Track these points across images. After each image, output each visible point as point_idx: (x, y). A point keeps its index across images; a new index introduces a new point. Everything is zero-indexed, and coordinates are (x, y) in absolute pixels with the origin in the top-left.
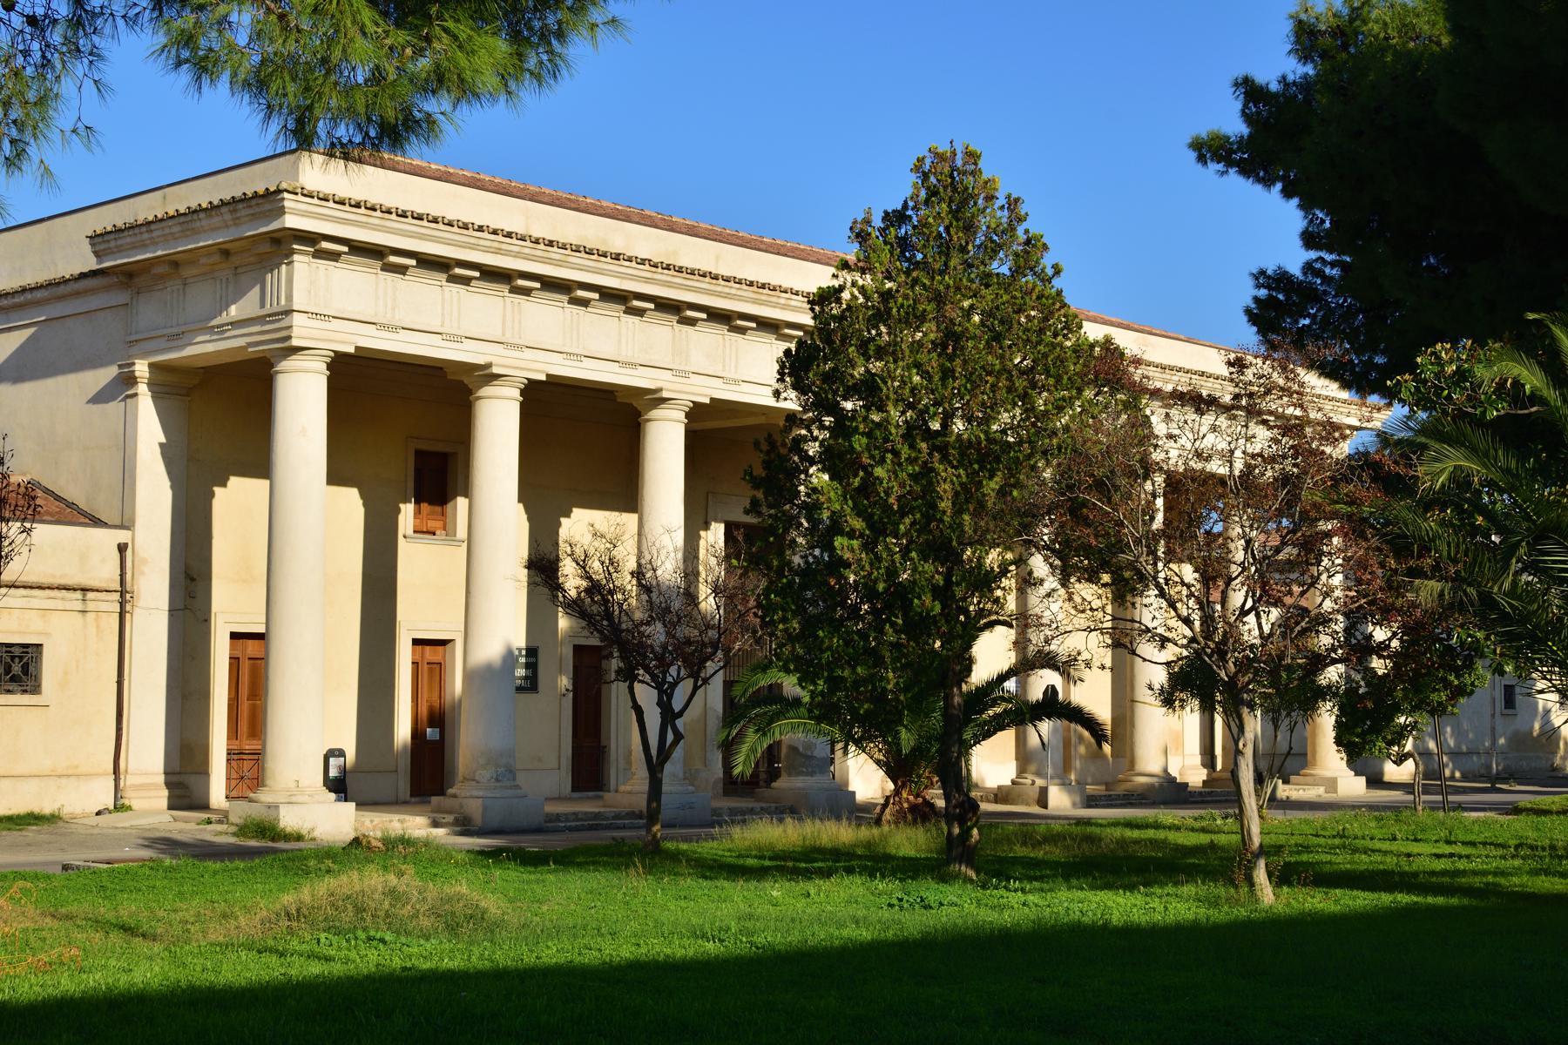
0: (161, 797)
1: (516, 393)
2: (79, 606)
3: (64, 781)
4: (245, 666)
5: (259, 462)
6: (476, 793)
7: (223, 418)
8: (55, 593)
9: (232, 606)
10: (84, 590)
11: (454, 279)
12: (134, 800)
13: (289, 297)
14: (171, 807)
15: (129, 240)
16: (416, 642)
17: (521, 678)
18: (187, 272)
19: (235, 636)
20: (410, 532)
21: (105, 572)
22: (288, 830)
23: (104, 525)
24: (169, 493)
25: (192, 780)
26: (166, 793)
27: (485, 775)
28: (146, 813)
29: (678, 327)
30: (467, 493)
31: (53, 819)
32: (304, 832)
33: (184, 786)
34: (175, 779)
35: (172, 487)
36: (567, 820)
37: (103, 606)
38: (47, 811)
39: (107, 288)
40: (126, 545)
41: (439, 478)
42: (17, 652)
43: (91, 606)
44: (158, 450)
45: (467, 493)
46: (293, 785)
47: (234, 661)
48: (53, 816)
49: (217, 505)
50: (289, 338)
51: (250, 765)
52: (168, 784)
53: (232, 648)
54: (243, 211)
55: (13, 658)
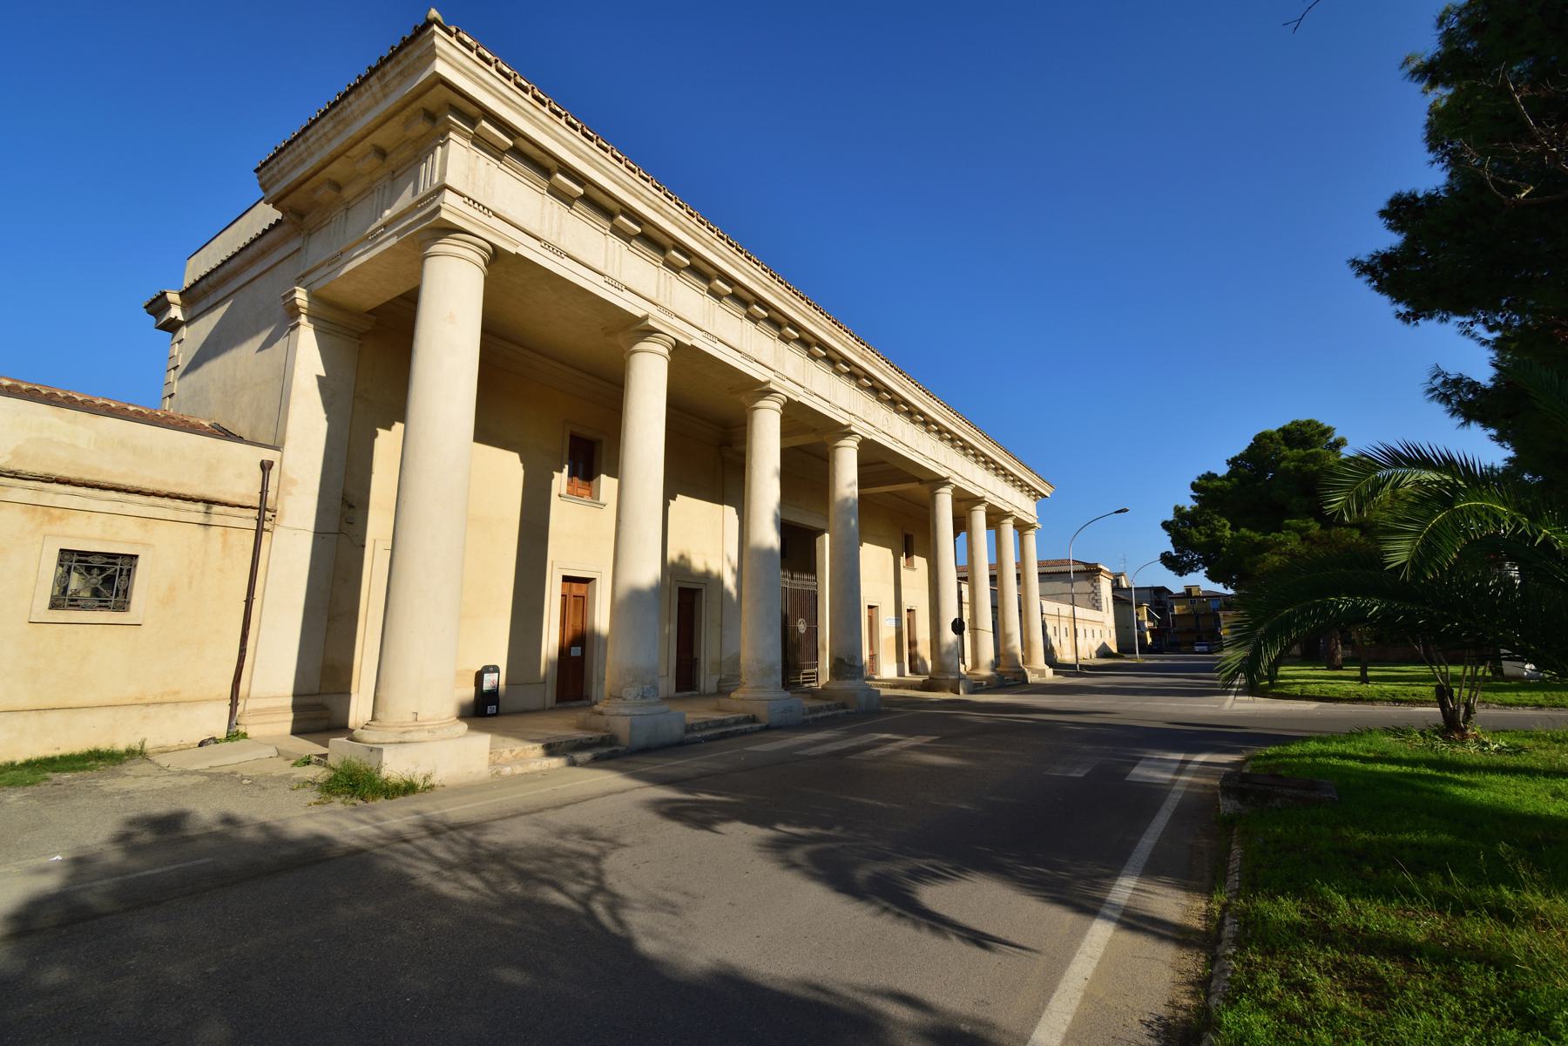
0: (286, 722)
1: (666, 352)
2: (201, 518)
3: (153, 710)
6: (622, 711)
8: (166, 501)
10: (209, 502)
11: (618, 231)
12: (253, 728)
13: (443, 174)
15: (288, 159)
18: (348, 193)
20: (564, 492)
21: (245, 487)
24: (325, 424)
26: (290, 716)
27: (631, 692)
29: (778, 342)
30: (615, 471)
32: (419, 781)
33: (320, 706)
35: (328, 419)
36: (701, 730)
38: (121, 746)
39: (285, 240)
40: (271, 464)
41: (592, 453)
42: (97, 561)
43: (215, 520)
44: (316, 382)
45: (615, 471)
46: (410, 718)
48: (131, 753)
50: (438, 209)
52: (295, 708)
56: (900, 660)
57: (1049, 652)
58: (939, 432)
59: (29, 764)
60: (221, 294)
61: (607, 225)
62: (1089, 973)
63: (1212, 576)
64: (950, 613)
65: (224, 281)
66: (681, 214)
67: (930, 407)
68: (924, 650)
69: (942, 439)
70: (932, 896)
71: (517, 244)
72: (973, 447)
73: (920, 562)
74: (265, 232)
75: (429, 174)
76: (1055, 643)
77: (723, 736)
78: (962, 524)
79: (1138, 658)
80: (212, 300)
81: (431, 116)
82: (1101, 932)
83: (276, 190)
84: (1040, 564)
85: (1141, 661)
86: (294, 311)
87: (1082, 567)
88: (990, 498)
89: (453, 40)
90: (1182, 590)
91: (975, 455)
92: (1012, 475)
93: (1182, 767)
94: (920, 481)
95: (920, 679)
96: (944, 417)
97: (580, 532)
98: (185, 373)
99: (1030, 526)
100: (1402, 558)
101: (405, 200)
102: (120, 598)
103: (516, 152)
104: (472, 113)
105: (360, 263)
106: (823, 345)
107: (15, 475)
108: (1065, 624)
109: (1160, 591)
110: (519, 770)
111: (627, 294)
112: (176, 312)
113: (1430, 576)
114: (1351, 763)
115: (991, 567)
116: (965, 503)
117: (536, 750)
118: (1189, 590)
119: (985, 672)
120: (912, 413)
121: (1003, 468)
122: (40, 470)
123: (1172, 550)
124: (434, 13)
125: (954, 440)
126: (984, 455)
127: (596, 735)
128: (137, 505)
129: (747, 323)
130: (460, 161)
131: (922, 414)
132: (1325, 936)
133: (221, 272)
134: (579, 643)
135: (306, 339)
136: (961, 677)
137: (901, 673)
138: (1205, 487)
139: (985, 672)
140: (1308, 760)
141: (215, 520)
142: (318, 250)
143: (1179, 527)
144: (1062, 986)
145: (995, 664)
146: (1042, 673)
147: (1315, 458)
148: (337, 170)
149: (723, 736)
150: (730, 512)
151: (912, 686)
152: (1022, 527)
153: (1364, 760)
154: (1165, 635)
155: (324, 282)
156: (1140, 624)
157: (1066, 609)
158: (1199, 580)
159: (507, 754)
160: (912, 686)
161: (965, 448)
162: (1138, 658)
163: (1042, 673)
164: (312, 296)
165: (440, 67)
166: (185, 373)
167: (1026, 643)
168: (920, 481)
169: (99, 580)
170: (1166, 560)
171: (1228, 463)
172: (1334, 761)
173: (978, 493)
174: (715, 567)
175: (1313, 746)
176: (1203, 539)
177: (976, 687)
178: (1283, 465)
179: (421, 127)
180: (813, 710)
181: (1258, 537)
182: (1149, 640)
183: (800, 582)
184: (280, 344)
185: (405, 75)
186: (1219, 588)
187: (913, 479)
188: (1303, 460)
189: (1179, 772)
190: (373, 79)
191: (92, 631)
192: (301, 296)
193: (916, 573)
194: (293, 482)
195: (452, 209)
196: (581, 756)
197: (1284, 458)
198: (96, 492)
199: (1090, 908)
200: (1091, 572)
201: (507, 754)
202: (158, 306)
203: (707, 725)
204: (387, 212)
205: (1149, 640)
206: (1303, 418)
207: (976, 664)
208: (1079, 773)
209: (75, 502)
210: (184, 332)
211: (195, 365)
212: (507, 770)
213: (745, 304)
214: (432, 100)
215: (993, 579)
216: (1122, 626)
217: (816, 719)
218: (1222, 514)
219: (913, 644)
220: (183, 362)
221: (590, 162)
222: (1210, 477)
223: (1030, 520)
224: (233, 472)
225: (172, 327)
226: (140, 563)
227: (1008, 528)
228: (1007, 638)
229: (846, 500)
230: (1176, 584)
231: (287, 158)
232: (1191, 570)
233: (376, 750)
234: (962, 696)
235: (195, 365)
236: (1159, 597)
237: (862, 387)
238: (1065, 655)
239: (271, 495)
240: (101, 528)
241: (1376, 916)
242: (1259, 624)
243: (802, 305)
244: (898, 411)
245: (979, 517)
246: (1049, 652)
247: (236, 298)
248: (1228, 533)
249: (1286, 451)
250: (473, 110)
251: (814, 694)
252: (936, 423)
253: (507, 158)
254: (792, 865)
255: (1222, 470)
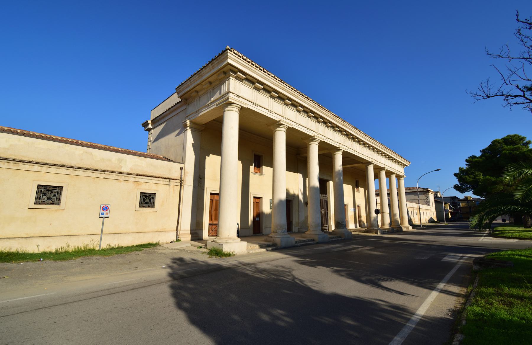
1: (285, 130)
2: (168, 183)
3: (160, 233)
4: (214, 202)
5: (218, 152)
7: (209, 138)
8: (161, 179)
9: (211, 186)
10: (170, 179)
12: (182, 238)
13: (228, 89)
14: (192, 240)
16: (254, 197)
17: (507, 175)
18: (200, 94)
19: (212, 194)
21: (176, 174)
22: (226, 253)
23: (171, 161)
25: (198, 232)
26: (190, 236)
27: (280, 231)
28: (186, 242)
31: (157, 245)
32: (231, 253)
33: (196, 234)
34: (193, 232)
37: (175, 184)
38: (154, 242)
39: (181, 106)
42: (148, 195)
43: (171, 183)
46: (227, 236)
47: (211, 200)
48: (156, 244)
49: (207, 160)
50: (229, 98)
51: (215, 229)
52: (191, 233)
53: (211, 197)
54: (215, 62)
55: (146, 197)
56: (355, 223)
57: (410, 221)
58: (369, 147)
59: (137, 246)
60: (162, 121)
61: (269, 95)
62: (432, 300)
63: (474, 193)
64: (374, 207)
65: (163, 117)
66: (289, 89)
67: (365, 139)
68: (364, 219)
69: (369, 149)
70: (384, 284)
71: (247, 104)
72: (380, 151)
73: (362, 190)
74: (176, 104)
75: (224, 88)
76: (412, 217)
77: (306, 245)
78: (377, 176)
79: (445, 223)
80: (160, 122)
81: (225, 73)
82: (434, 294)
83: (181, 94)
84: (406, 189)
85: (446, 224)
86: (186, 126)
87: (422, 190)
88: (387, 168)
89: (232, 53)
90: (463, 198)
91: (381, 154)
92: (395, 159)
93: (461, 258)
94: (362, 163)
95: (364, 229)
96: (371, 142)
97: (261, 183)
98: (154, 142)
99: (402, 177)
100: (520, 196)
101: (217, 95)
102: (57, 201)
103: (247, 79)
104: (235, 70)
105: (205, 113)
106: (331, 123)
107: (131, 174)
108: (415, 211)
109: (455, 198)
110: (254, 252)
111: (275, 115)
112: (150, 126)
113: (527, 202)
114: (522, 258)
115: (388, 190)
116: (378, 170)
117: (257, 246)
118: (466, 198)
119: (387, 227)
120: (359, 141)
121: (391, 157)
122: (136, 173)
123: (458, 184)
124: (228, 47)
125: (374, 149)
126: (384, 153)
127: (271, 243)
128: (155, 180)
129: (307, 118)
130: (236, 88)
131: (363, 141)
132: (499, 294)
133: (163, 115)
134: (259, 215)
135: (189, 132)
136: (378, 229)
137: (356, 227)
138: (471, 161)
139: (387, 227)
140: (507, 256)
141: (171, 183)
142: (191, 109)
143: (461, 175)
144: (425, 302)
145: (390, 224)
146: (408, 228)
147: (517, 149)
148: (198, 88)
149: (306, 245)
150: (300, 176)
151: (361, 231)
152: (399, 177)
153: (527, 256)
154: (454, 214)
155: (194, 118)
156: (446, 211)
157: (416, 205)
158: (470, 194)
159: (249, 247)
160: (361, 231)
161: (378, 151)
162: (445, 223)
163: (408, 228)
164: (191, 122)
165: (229, 61)
166: (154, 142)
167: (402, 217)
168: (362, 163)
169: (49, 195)
170: (456, 187)
171: (481, 151)
172: (517, 257)
173: (382, 166)
174: (296, 193)
175: (510, 252)
176: (471, 180)
177: (384, 232)
178: (504, 152)
179: (222, 76)
180: (331, 238)
181: (494, 179)
182: (450, 217)
183: (323, 197)
184: (182, 135)
185: (219, 63)
186: (479, 197)
187: (359, 162)
188: (512, 150)
189: (460, 259)
190: (210, 64)
191: (46, 212)
192: (188, 122)
193: (361, 193)
194: (188, 173)
195: (232, 98)
196: (270, 249)
197: (504, 149)
198: (147, 178)
199: (433, 289)
200: (426, 192)
201: (249, 247)
202: (145, 124)
203: (300, 241)
204: (212, 99)
205: (450, 217)
206: (512, 134)
207: (383, 224)
208: (425, 258)
209: (143, 180)
210: (152, 131)
211: (156, 139)
212: (251, 252)
213: (307, 113)
214: (225, 69)
215: (388, 194)
216: (439, 211)
217: (332, 241)
218: (479, 170)
219: (360, 217)
220: (152, 140)
221: (265, 79)
222: (474, 157)
223: (402, 174)
224: (173, 170)
225: (149, 130)
226: (156, 195)
227: (394, 178)
228: (395, 215)
229: (339, 171)
230: (461, 196)
231: (185, 86)
232: (467, 191)
233: (221, 245)
234: (379, 234)
235: (156, 139)
236: (454, 200)
237: (343, 134)
238: (416, 222)
239: (183, 176)
240: (148, 187)
241: (514, 291)
242: (521, 205)
243: (324, 111)
244: (354, 141)
245: (383, 174)
246: (410, 221)
247: (168, 122)
248: (481, 177)
249: (505, 146)
250: (236, 70)
251: (330, 233)
252: (368, 144)
253: (244, 81)
254: (342, 276)
255: (478, 154)
